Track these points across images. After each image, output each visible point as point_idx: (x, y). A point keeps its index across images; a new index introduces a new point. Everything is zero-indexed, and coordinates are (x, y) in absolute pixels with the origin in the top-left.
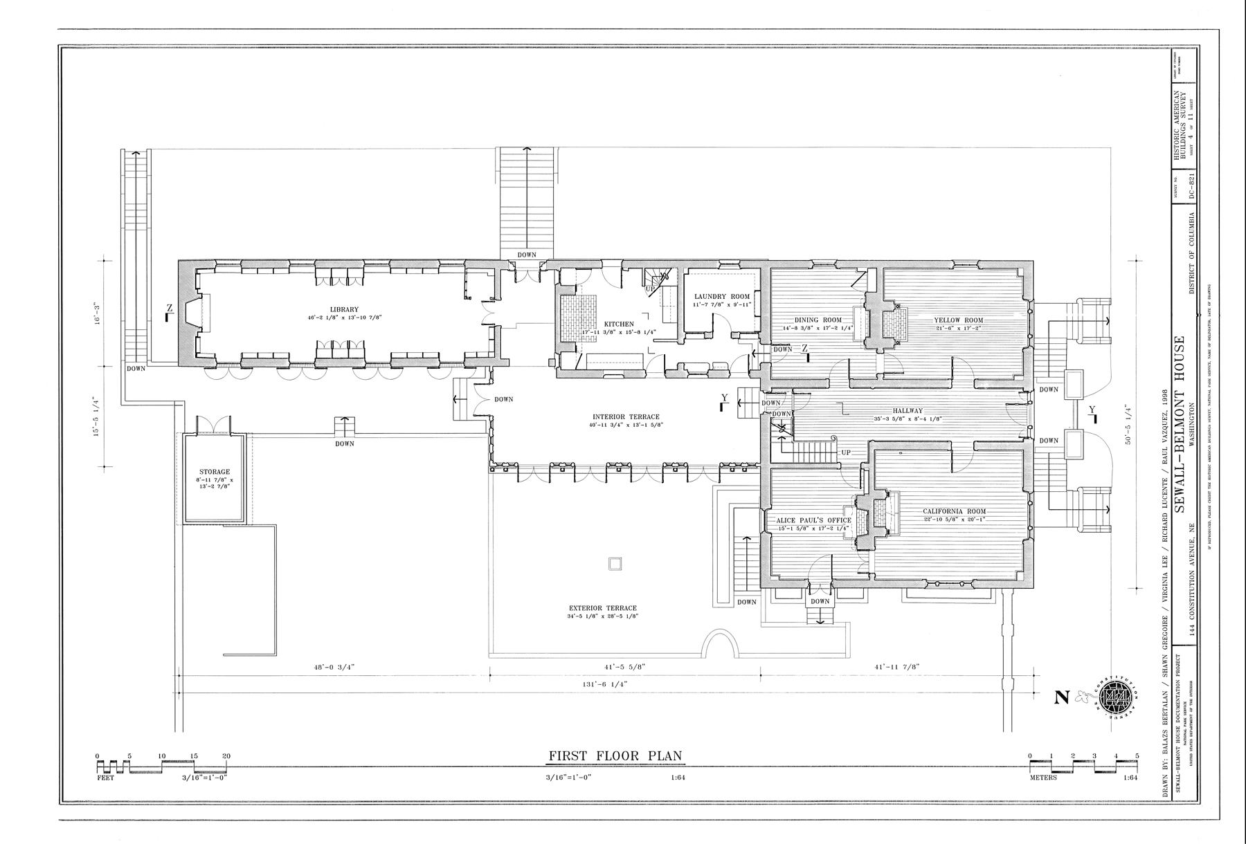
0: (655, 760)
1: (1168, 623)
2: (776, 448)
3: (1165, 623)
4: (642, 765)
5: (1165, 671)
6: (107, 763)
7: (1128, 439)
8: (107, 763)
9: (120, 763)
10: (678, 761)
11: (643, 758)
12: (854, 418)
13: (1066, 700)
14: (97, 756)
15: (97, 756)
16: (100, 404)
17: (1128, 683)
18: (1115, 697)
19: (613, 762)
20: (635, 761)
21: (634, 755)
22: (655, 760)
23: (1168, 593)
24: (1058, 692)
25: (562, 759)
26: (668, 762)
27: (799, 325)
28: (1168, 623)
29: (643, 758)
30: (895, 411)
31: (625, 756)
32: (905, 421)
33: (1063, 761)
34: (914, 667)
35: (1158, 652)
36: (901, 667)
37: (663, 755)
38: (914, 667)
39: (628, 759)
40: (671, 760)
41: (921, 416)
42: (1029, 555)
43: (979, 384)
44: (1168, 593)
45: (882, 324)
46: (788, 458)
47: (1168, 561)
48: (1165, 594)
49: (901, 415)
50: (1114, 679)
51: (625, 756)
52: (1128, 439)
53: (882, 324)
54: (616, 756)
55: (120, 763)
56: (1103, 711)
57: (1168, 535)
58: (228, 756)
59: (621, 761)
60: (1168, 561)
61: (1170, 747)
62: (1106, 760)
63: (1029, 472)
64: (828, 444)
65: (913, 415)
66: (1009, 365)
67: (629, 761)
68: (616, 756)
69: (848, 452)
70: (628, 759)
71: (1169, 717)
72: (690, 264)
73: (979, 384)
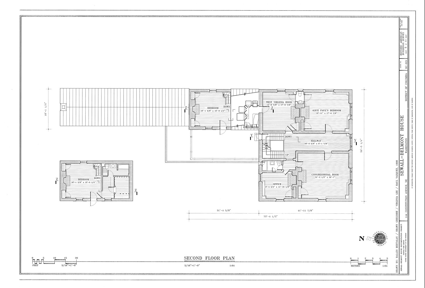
0: (225, 259)
1: (398, 213)
2: (264, 153)
3: (397, 213)
4: (205, 261)
5: (397, 230)
6: (36, 260)
7: (361, 150)
8: (36, 260)
9: (40, 260)
10: (233, 260)
11: (221, 259)
12: (295, 143)
13: (363, 239)
14: (32, 258)
15: (32, 258)
16: (363, 141)
17: (384, 234)
18: (380, 238)
19: (211, 260)
20: (219, 260)
21: (218, 258)
22: (225, 259)
23: (398, 203)
24: (360, 237)
25: (187, 259)
26: (230, 260)
27: (332, 112)
28: (398, 213)
29: (221, 259)
30: (312, 141)
31: (215, 258)
32: (315, 144)
33: (362, 260)
34: (311, 211)
35: (394, 223)
36: (307, 211)
37: (228, 258)
38: (311, 211)
39: (216, 259)
40: (230, 260)
41: (321, 143)
42: (350, 189)
43: (333, 132)
44: (398, 203)
45: (300, 112)
46: (269, 157)
47: (398, 192)
48: (397, 203)
49: (314, 142)
50: (379, 232)
51: (215, 258)
52: (361, 150)
53: (300, 112)
54: (212, 258)
55: (40, 260)
56: (375, 243)
57: (398, 183)
58: (77, 258)
59: (214, 260)
60: (398, 192)
61: (399, 256)
62: (376, 260)
63: (350, 162)
64: (281, 152)
65: (318, 142)
66: (342, 126)
67: (217, 260)
68: (212, 258)
69: (288, 155)
70: (216, 259)
71: (398, 245)
72: (263, 91)
73: (333, 132)
